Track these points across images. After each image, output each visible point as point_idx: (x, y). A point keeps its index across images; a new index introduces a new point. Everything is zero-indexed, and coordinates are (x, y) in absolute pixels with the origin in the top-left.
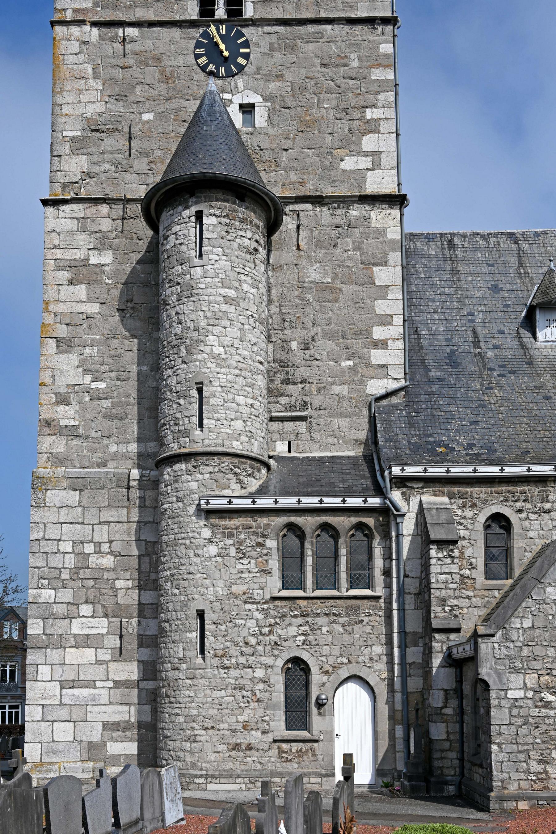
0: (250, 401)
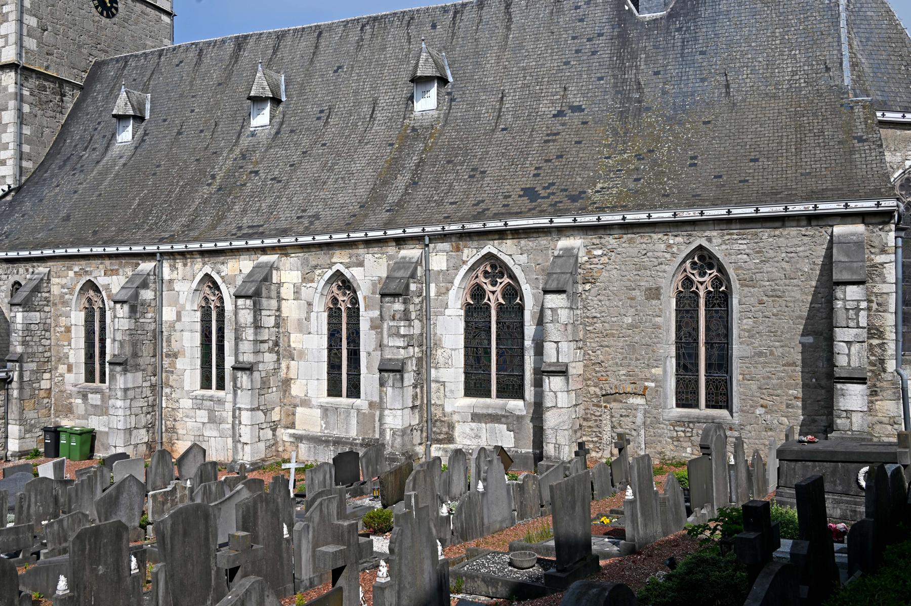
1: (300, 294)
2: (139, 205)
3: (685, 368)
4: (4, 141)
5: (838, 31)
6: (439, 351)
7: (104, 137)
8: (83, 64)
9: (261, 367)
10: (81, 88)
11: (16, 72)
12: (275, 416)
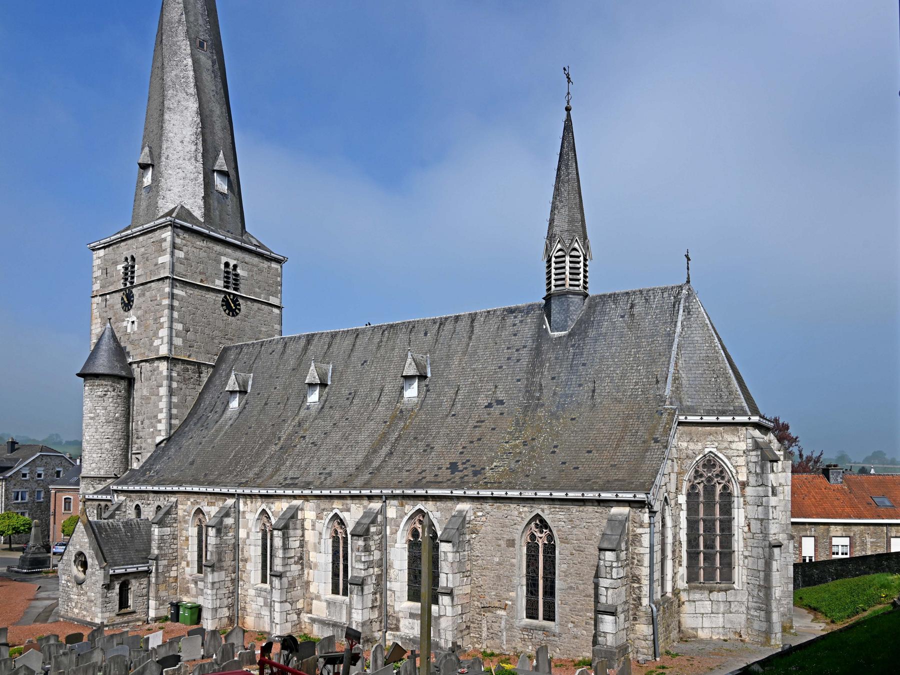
1: (315, 528)
3: (532, 593)
5: (670, 352)
6: (392, 571)
8: (215, 350)
9: (288, 574)
12: (300, 605)
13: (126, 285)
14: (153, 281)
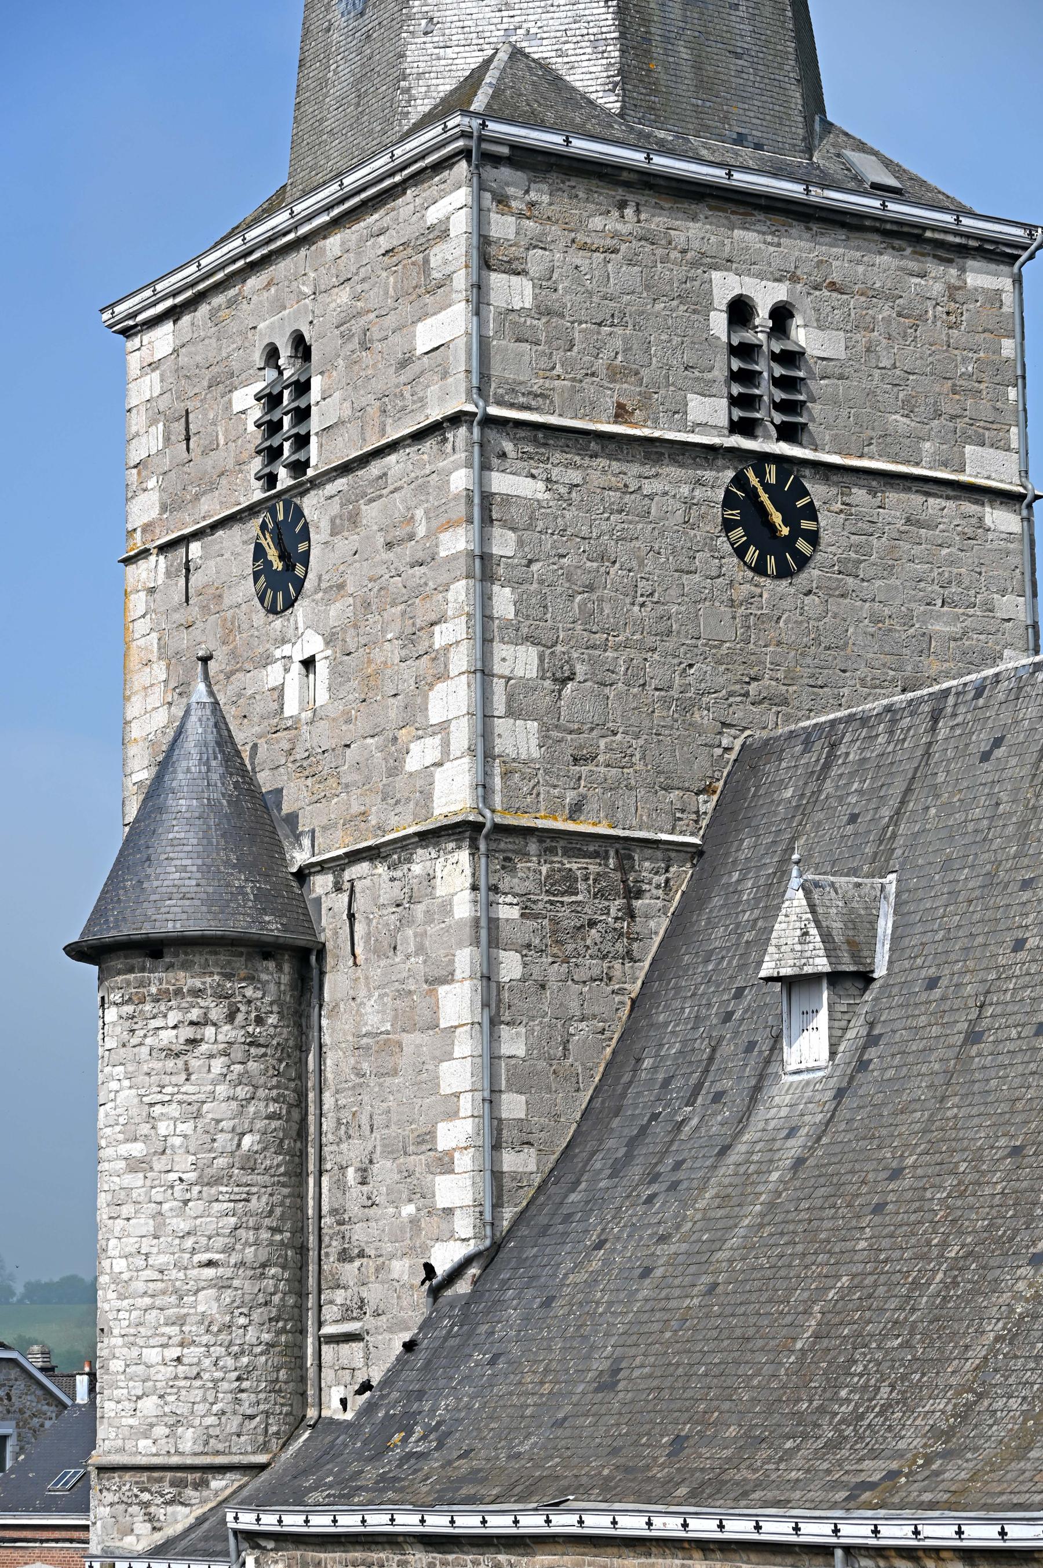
0: (176, 1352)
2: (817, 1336)
4: (445, 1089)
7: (751, 1046)
8: (702, 765)
10: (696, 853)
11: (474, 848)
13: (271, 480)
14: (393, 447)
